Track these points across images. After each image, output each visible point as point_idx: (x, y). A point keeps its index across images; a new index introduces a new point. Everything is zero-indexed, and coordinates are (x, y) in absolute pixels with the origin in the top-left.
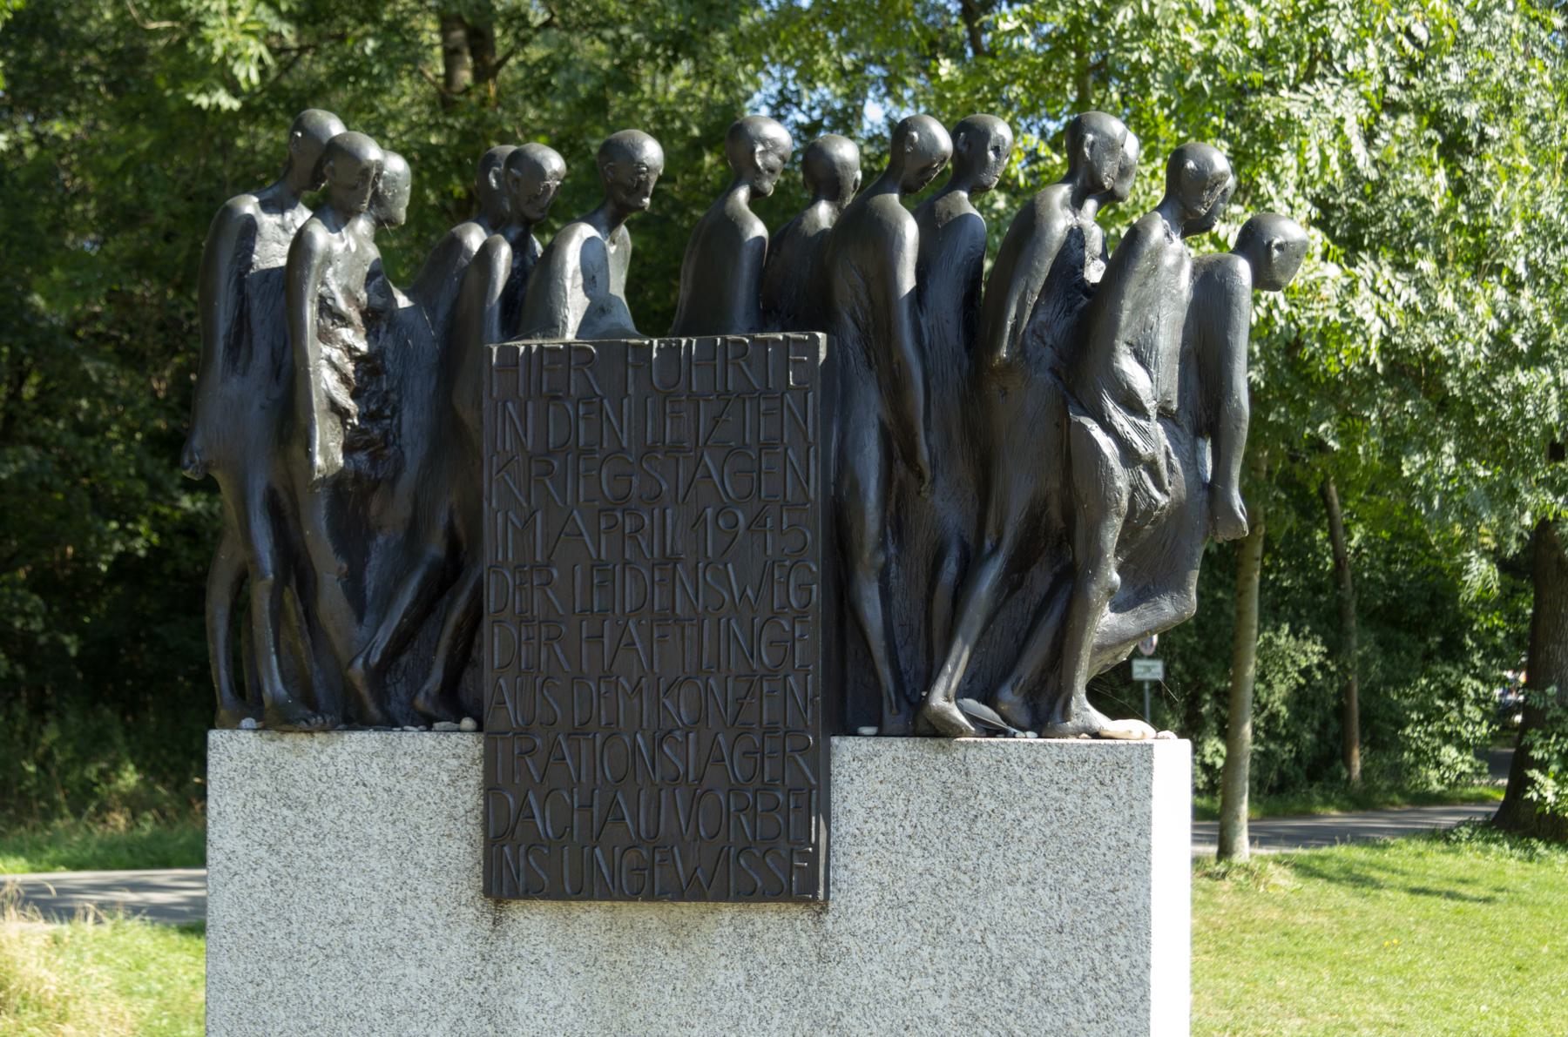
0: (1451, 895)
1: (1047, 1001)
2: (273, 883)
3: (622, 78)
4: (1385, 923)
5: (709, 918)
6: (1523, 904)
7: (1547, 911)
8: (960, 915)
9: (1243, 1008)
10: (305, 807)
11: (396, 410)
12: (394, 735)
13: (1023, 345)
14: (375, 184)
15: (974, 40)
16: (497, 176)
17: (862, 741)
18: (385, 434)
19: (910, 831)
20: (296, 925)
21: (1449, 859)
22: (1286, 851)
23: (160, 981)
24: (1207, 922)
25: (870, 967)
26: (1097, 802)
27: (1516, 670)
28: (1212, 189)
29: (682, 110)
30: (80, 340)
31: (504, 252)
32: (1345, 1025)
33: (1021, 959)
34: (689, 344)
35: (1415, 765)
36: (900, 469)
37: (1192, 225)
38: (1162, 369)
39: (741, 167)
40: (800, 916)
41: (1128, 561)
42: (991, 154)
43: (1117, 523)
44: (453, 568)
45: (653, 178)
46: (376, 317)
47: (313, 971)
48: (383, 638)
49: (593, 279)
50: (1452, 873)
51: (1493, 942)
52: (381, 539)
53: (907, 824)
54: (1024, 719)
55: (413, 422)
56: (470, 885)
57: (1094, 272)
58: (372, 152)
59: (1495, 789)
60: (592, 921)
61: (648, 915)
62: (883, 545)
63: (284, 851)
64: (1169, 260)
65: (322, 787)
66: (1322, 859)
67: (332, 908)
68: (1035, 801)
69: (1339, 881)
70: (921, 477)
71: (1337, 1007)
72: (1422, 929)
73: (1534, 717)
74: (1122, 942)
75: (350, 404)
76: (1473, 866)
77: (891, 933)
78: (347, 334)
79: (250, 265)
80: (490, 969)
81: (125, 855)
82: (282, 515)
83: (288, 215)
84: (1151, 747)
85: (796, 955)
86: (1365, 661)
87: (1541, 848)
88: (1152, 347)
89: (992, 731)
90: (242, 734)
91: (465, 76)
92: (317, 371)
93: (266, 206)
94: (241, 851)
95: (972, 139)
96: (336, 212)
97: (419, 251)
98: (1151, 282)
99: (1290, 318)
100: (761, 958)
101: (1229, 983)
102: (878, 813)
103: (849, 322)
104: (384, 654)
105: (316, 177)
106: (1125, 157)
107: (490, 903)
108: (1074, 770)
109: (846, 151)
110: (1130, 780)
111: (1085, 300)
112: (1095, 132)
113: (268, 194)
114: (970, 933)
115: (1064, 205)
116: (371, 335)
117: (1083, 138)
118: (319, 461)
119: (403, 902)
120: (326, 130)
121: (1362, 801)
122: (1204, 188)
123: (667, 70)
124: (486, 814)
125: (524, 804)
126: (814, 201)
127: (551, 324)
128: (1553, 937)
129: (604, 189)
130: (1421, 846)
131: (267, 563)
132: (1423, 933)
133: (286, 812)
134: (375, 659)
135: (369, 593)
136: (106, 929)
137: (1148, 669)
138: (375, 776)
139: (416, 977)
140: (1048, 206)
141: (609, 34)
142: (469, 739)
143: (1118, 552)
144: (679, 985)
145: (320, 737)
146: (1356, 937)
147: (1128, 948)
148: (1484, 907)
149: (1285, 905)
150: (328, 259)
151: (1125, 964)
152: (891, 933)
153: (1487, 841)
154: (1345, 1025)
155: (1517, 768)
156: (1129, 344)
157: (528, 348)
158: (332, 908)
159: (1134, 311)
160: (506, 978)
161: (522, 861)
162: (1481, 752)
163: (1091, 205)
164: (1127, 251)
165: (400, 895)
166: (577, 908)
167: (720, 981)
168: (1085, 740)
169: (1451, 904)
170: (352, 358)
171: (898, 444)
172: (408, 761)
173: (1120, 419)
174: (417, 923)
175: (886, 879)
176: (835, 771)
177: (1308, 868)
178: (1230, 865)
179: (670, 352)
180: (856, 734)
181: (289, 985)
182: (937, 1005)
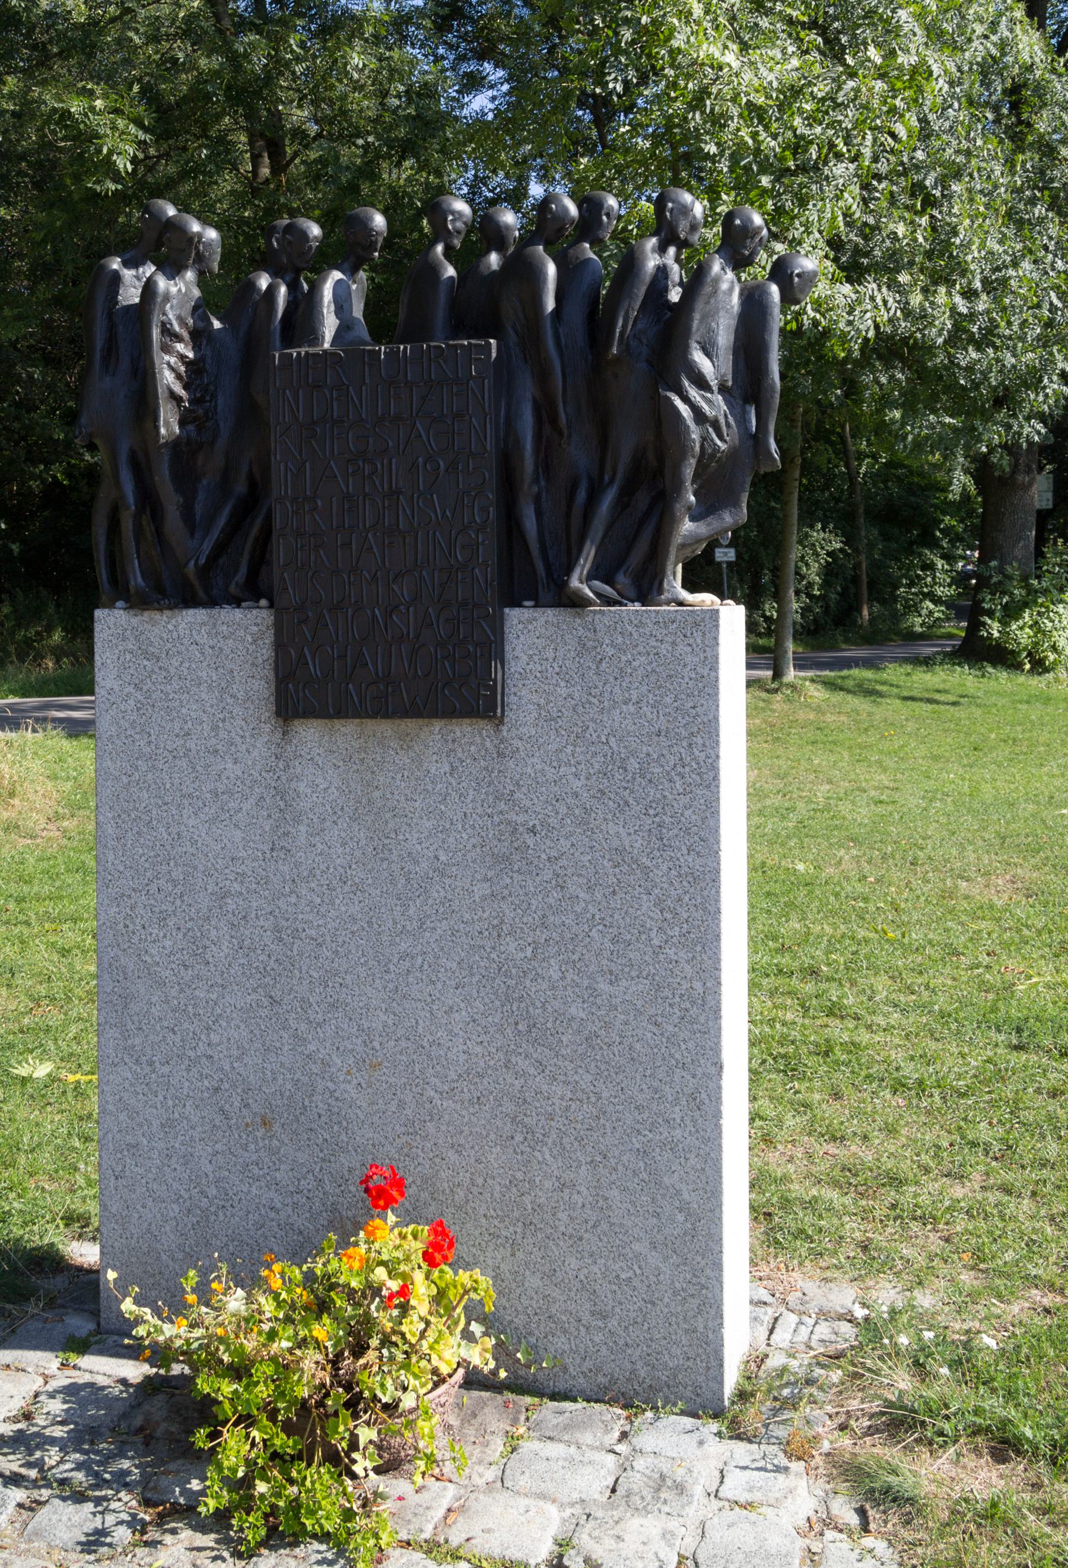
0: (930, 701)
1: (650, 781)
2: (138, 709)
3: (369, 171)
4: (885, 720)
5: (425, 729)
6: (978, 706)
7: (994, 710)
8: (592, 725)
9: (790, 779)
10: (158, 659)
11: (214, 396)
12: (215, 611)
13: (628, 345)
14: (197, 248)
15: (602, 137)
16: (277, 240)
17: (525, 610)
18: (207, 412)
19: (557, 669)
20: (153, 737)
21: (928, 676)
22: (819, 673)
23: (75, 770)
24: (765, 722)
25: (532, 760)
26: (682, 648)
27: (972, 550)
28: (752, 238)
29: (409, 190)
30: (18, 350)
31: (283, 289)
32: (859, 789)
33: (633, 754)
34: (405, 349)
35: (905, 614)
36: (547, 430)
37: (739, 262)
38: (721, 359)
39: (440, 232)
40: (485, 727)
41: (700, 487)
42: (604, 218)
43: (693, 462)
44: (253, 500)
45: (380, 240)
46: (199, 336)
47: (166, 767)
48: (207, 547)
49: (341, 306)
50: (930, 684)
51: (958, 731)
52: (205, 482)
53: (555, 665)
54: (632, 594)
55: (224, 402)
56: (267, 711)
57: (675, 295)
58: (196, 227)
59: (958, 629)
60: (347, 732)
61: (384, 728)
62: (536, 480)
63: (145, 688)
64: (724, 286)
65: (169, 645)
66: (843, 678)
67: (177, 725)
68: (641, 648)
69: (854, 693)
70: (561, 434)
71: (853, 777)
72: (910, 724)
73: (984, 582)
74: (700, 741)
75: (183, 393)
76: (944, 681)
77: (546, 737)
78: (180, 347)
79: (117, 303)
80: (281, 765)
81: (52, 687)
82: (140, 467)
83: (141, 270)
84: (717, 611)
85: (483, 753)
86: (871, 546)
87: (990, 670)
88: (713, 344)
89: (609, 602)
90: (116, 611)
91: (265, 171)
92: (161, 372)
93: (126, 264)
94: (117, 688)
95: (591, 207)
96: (172, 268)
97: (226, 293)
98: (712, 301)
99: (816, 323)
100: (460, 755)
101: (781, 762)
102: (536, 658)
103: (512, 332)
104: (208, 558)
105: (159, 244)
106: (694, 217)
107: (281, 721)
108: (666, 627)
109: (509, 218)
110: (704, 634)
111: (669, 314)
112: (673, 202)
113: (128, 256)
114: (599, 737)
115: (653, 251)
116: (196, 348)
117: (666, 206)
118: (163, 431)
119: (224, 721)
120: (166, 213)
121: (872, 638)
122: (747, 237)
123: (399, 165)
124: (276, 662)
125: (302, 655)
126: (488, 252)
127: (315, 337)
128: (999, 728)
129: (347, 247)
130: (909, 668)
131: (131, 499)
132: (911, 726)
133: (146, 662)
134: (202, 561)
135: (198, 518)
136: (40, 735)
137: (726, 554)
138: (203, 638)
139: (233, 770)
140: (643, 252)
141: (360, 142)
142: (265, 613)
143: (693, 482)
144: (406, 773)
145: (167, 613)
146: (866, 730)
147: (704, 745)
148: (952, 709)
149: (818, 710)
150: (167, 297)
151: (703, 755)
152: (546, 737)
153: (954, 664)
154: (859, 789)
155: (974, 615)
156: (699, 343)
157: (299, 354)
158: (177, 725)
159: (701, 321)
160: (292, 770)
161: (304, 691)
162: (949, 604)
163: (672, 251)
164: (696, 279)
165: (221, 716)
166: (337, 723)
167: (433, 771)
168: (673, 608)
169: (930, 707)
170: (184, 363)
171: (545, 412)
172: (225, 628)
173: (693, 393)
174: (233, 734)
175: (542, 701)
176: (507, 631)
177: (833, 684)
178: (781, 683)
179: (392, 354)
180: (520, 606)
181: (150, 776)
182: (576, 784)
